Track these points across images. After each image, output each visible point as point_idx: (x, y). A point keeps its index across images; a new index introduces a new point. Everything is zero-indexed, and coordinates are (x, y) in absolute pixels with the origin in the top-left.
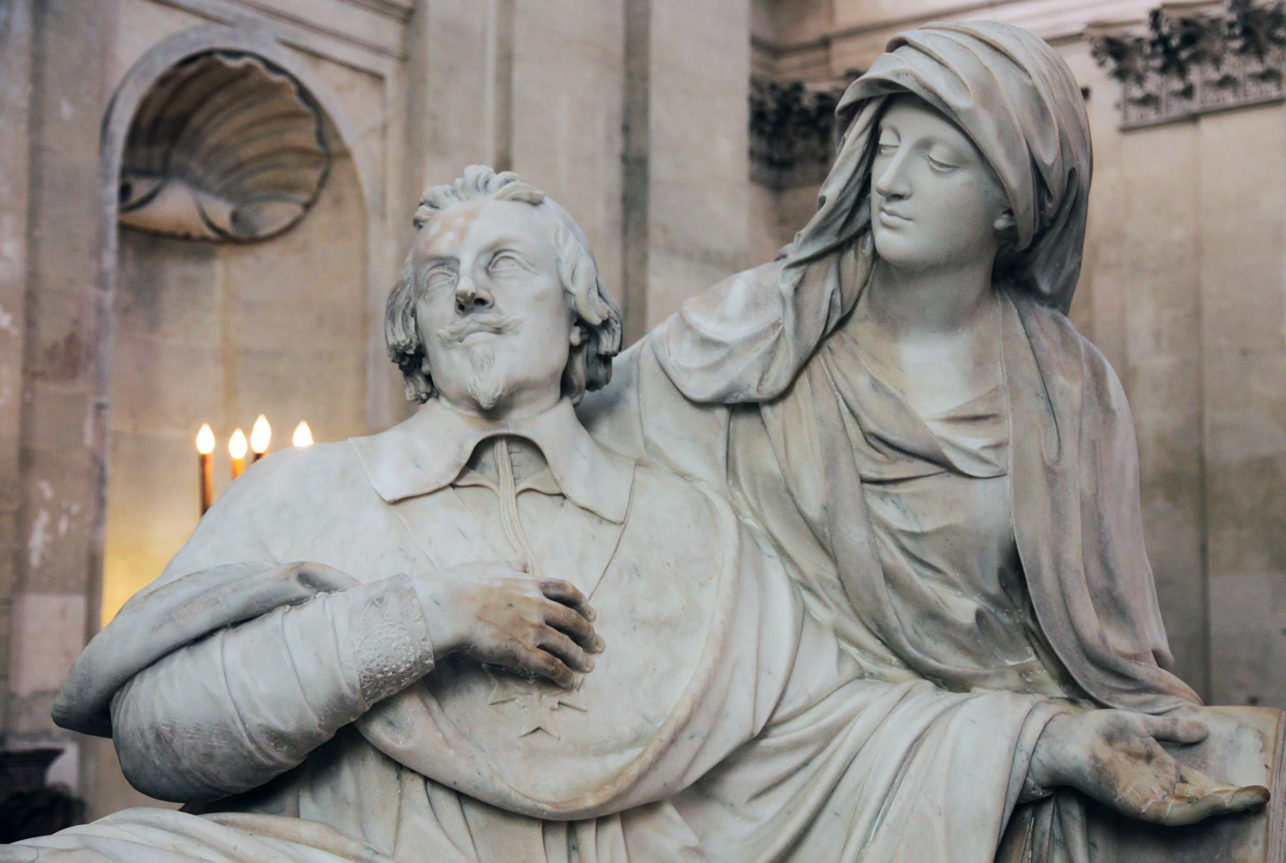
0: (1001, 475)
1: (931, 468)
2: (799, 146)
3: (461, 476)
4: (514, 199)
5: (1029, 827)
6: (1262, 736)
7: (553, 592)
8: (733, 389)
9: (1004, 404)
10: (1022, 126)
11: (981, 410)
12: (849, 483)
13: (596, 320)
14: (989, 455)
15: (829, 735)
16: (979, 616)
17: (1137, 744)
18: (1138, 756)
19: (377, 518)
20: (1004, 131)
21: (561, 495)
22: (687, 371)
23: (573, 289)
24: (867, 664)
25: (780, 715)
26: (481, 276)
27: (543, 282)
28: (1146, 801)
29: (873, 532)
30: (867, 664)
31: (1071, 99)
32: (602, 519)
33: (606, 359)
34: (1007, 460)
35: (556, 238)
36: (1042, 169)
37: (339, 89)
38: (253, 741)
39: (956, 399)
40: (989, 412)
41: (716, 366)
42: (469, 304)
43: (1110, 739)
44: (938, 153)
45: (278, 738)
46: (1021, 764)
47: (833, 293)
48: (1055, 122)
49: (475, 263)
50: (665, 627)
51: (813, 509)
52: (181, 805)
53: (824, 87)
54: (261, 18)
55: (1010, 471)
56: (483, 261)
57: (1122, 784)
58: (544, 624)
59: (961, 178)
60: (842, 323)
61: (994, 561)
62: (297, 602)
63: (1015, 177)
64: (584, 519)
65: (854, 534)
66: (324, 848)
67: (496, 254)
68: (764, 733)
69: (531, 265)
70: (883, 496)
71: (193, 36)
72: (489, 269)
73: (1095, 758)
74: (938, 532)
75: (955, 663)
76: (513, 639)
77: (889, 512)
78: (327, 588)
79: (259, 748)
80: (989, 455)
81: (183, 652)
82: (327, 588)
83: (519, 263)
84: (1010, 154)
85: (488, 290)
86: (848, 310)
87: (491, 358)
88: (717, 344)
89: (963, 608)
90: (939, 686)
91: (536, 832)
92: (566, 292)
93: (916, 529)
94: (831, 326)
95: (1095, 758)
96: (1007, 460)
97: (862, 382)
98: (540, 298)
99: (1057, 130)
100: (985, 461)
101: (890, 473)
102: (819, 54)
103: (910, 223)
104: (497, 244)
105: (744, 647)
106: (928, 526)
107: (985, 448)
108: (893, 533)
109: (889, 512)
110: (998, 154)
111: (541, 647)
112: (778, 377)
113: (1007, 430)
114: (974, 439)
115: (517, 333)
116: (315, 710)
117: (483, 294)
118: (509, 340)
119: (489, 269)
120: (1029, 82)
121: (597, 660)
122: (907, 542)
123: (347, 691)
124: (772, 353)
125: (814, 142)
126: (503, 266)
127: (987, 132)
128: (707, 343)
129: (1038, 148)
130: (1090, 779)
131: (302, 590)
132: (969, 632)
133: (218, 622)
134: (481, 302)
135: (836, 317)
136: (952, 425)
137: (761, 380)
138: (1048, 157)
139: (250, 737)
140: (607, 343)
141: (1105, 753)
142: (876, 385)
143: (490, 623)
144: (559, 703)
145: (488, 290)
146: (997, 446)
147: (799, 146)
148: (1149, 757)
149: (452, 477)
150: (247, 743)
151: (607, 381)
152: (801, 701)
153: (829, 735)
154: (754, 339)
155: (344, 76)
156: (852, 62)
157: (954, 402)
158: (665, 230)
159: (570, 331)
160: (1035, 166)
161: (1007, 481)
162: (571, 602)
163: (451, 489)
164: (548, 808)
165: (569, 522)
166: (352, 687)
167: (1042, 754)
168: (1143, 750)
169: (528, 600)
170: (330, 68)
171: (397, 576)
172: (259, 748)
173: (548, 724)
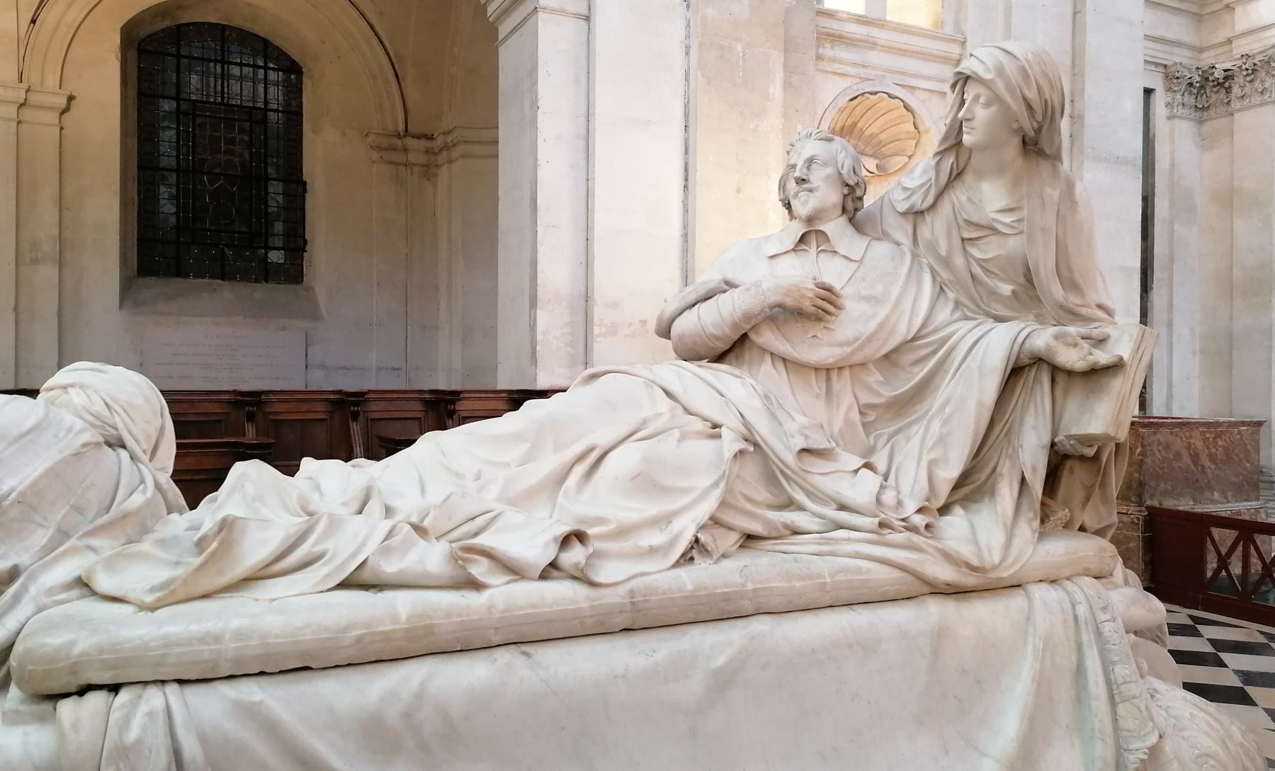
0: (1021, 233)
1: (991, 233)
3: (796, 246)
4: (820, 140)
7: (819, 286)
8: (912, 206)
10: (1016, 83)
11: (1012, 206)
12: (957, 242)
13: (852, 183)
14: (1015, 224)
15: (944, 340)
16: (1014, 292)
17: (1070, 340)
20: (1009, 86)
21: (835, 251)
22: (899, 201)
23: (843, 172)
24: (969, 314)
25: (924, 332)
26: (805, 170)
27: (829, 170)
31: (1044, 68)
32: (851, 260)
33: (861, 199)
34: (1024, 227)
35: (836, 153)
36: (1029, 100)
39: (1002, 203)
40: (1016, 206)
41: (909, 197)
42: (801, 181)
43: (1056, 337)
44: (982, 100)
45: (717, 338)
46: (1016, 348)
49: (803, 165)
50: (874, 300)
51: (943, 253)
53: (1228, 65)
54: (887, 74)
57: (1058, 356)
58: (814, 297)
59: (993, 109)
60: (959, 175)
61: (1020, 270)
62: (724, 291)
63: (1016, 106)
64: (843, 260)
65: (959, 261)
66: (727, 373)
67: (810, 161)
68: (914, 339)
69: (825, 164)
71: (855, 87)
72: (808, 168)
73: (1048, 345)
75: (1003, 312)
76: (800, 302)
78: (735, 286)
79: (710, 341)
80: (1015, 224)
81: (687, 311)
82: (735, 286)
83: (819, 164)
84: (1013, 96)
85: (807, 176)
86: (960, 170)
89: (1006, 289)
90: (306, 192)
91: (813, 373)
92: (840, 174)
93: (985, 257)
94: (953, 177)
95: (1048, 345)
96: (1024, 227)
97: (964, 198)
98: (828, 177)
100: (1012, 227)
101: (974, 235)
102: (1226, 48)
106: (990, 256)
107: (1013, 221)
108: (977, 260)
109: (975, 252)
111: (813, 306)
112: (930, 200)
113: (1024, 213)
114: (1007, 219)
115: (817, 191)
117: (805, 177)
119: (808, 168)
120: (1020, 64)
121: (843, 312)
122: (983, 264)
123: (737, 320)
124: (928, 191)
125: (1222, 94)
126: (814, 166)
127: (1000, 86)
128: (905, 189)
131: (726, 287)
132: (1008, 298)
133: (699, 299)
135: (955, 173)
137: (922, 202)
138: (1032, 94)
139: (707, 336)
140: (859, 193)
141: (1053, 343)
142: (969, 200)
143: (790, 296)
144: (824, 327)
145: (807, 176)
146: (1019, 221)
147: (1212, 100)
148: (1075, 345)
149: (792, 247)
150: (706, 339)
152: (931, 328)
155: (926, 95)
159: (842, 189)
160: (1025, 99)
162: (829, 289)
163: (792, 252)
164: (813, 363)
165: (838, 262)
166: (739, 319)
167: (1027, 345)
168: (1072, 342)
169: (807, 289)
171: (694, 268)
172: (710, 341)
173: (819, 335)
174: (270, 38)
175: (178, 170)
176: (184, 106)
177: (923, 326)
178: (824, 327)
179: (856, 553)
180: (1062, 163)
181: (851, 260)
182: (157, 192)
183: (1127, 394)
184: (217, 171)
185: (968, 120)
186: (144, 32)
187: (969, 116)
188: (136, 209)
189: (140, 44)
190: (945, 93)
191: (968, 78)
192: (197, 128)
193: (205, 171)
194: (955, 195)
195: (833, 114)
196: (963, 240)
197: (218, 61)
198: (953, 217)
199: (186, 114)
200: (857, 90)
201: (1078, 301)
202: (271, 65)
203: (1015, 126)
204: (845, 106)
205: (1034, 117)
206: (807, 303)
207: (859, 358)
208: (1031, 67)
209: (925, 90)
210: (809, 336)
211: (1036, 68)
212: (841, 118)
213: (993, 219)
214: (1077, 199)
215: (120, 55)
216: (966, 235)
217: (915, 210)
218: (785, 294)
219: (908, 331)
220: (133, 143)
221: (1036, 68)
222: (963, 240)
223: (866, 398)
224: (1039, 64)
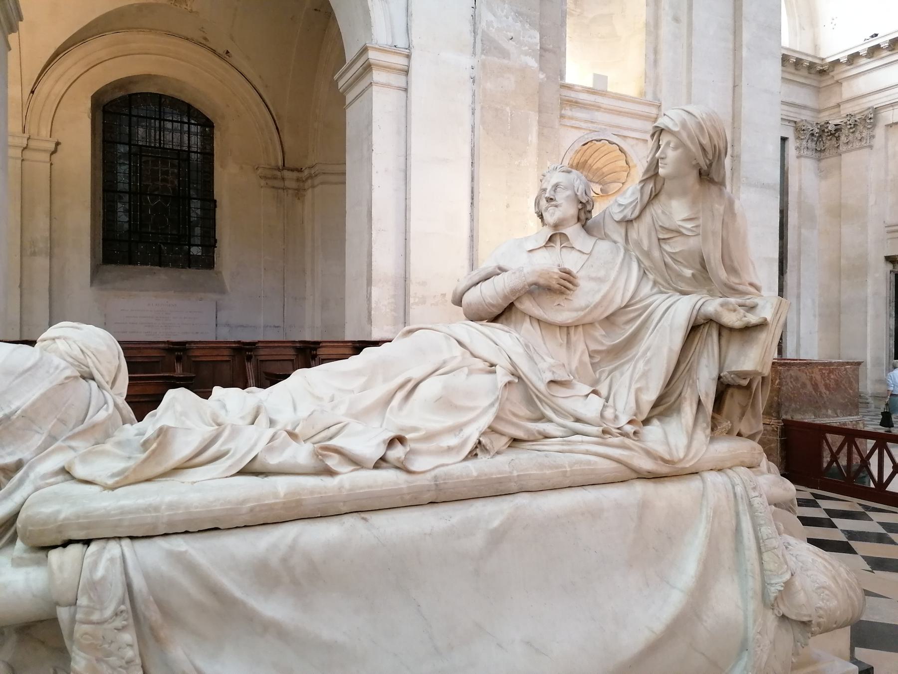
2: (828, 143)
3: (546, 244)
4: (563, 172)
5: (701, 331)
6: (772, 304)
7: (563, 270)
9: (701, 214)
11: (693, 216)
14: (694, 229)
15: (650, 305)
16: (693, 275)
17: (731, 307)
18: (731, 310)
19: (525, 255)
20: (690, 136)
23: (578, 194)
24: (663, 289)
26: (552, 193)
28: (730, 322)
29: (662, 253)
30: (663, 289)
31: (713, 123)
32: (583, 253)
33: (590, 212)
34: (700, 230)
35: (574, 181)
37: (632, 146)
38: (487, 306)
41: (622, 211)
42: (549, 200)
44: (672, 145)
45: (493, 305)
46: (695, 312)
47: (652, 188)
48: (706, 130)
51: (646, 249)
52: (486, 321)
55: (701, 233)
56: (553, 189)
59: (680, 151)
60: (656, 195)
61: (698, 260)
62: (498, 274)
63: (695, 149)
67: (556, 187)
68: (626, 306)
69: (566, 188)
70: (665, 243)
71: (586, 136)
74: (680, 252)
75: (685, 288)
76: (549, 281)
77: (667, 248)
78: (505, 271)
80: (694, 229)
82: (505, 271)
84: (692, 143)
86: (657, 192)
87: (554, 213)
88: (622, 205)
89: (688, 273)
93: (674, 251)
94: (652, 197)
96: (700, 230)
97: (659, 212)
99: (707, 134)
100: (692, 231)
101: (666, 236)
102: (836, 110)
103: (665, 166)
104: (557, 183)
105: (621, 284)
106: (677, 250)
107: (692, 227)
108: (668, 253)
109: (667, 248)
110: (689, 143)
111: (558, 284)
112: (637, 213)
113: (700, 222)
114: (689, 225)
116: (500, 298)
117: (552, 197)
118: (560, 208)
120: (697, 121)
121: (578, 288)
122: (673, 256)
124: (635, 206)
125: (834, 141)
127: (684, 135)
128: (620, 205)
129: (701, 139)
130: (714, 316)
131: (499, 271)
132: (689, 279)
133: (480, 280)
134: (551, 199)
135: (653, 194)
136: (684, 222)
138: (705, 141)
140: (589, 208)
141: (720, 309)
142: (663, 212)
146: (697, 226)
147: (828, 143)
148: (735, 311)
149: (544, 244)
150: (486, 307)
151: (591, 218)
153: (650, 305)
154: (631, 203)
155: (634, 142)
156: (849, 111)
157: (685, 215)
158: (747, 178)
160: (701, 145)
161: (700, 237)
162: (569, 273)
165: (575, 254)
166: (508, 293)
167: (702, 310)
170: (629, 140)
174: (192, 103)
175: (130, 193)
176: (134, 149)
177: (632, 297)
178: (565, 298)
179: (587, 451)
180: (726, 188)
181: (583, 253)
182: (116, 208)
183: (770, 343)
184: (156, 193)
185: (662, 158)
186: (107, 99)
187: (663, 156)
188: (102, 219)
189: (104, 107)
190: (647, 141)
191: (662, 130)
192: (143, 164)
193: (148, 193)
194: (654, 210)
195: (572, 154)
196: (659, 239)
197: (186, 123)
198: (652, 224)
199: (135, 154)
200: (588, 138)
201: (737, 281)
202: (193, 122)
203: (694, 162)
204: (580, 149)
205: (707, 157)
206: (554, 282)
207: (588, 319)
208: (705, 124)
209: (633, 138)
210: (555, 305)
211: (708, 123)
212: (577, 157)
213: (679, 226)
214: (736, 211)
215: (91, 114)
216: (661, 236)
217: (627, 219)
218: (539, 276)
219: (622, 301)
220: (100, 174)
221: (708, 123)
222: (659, 239)
223: (594, 346)
224: (710, 120)
